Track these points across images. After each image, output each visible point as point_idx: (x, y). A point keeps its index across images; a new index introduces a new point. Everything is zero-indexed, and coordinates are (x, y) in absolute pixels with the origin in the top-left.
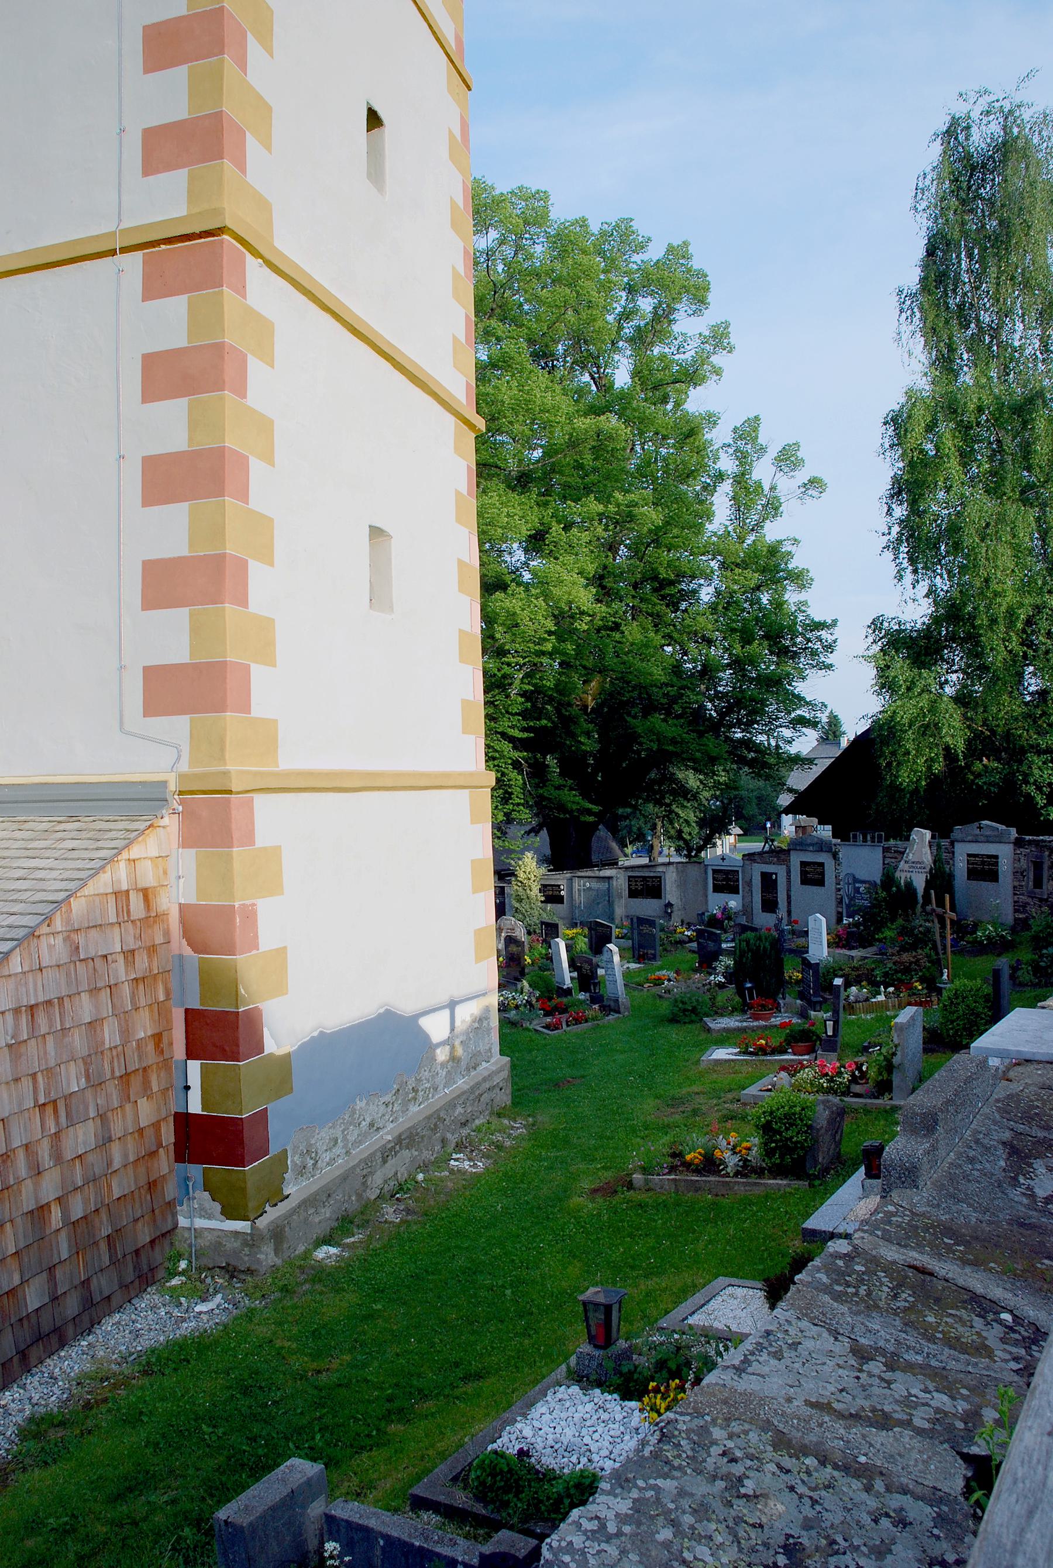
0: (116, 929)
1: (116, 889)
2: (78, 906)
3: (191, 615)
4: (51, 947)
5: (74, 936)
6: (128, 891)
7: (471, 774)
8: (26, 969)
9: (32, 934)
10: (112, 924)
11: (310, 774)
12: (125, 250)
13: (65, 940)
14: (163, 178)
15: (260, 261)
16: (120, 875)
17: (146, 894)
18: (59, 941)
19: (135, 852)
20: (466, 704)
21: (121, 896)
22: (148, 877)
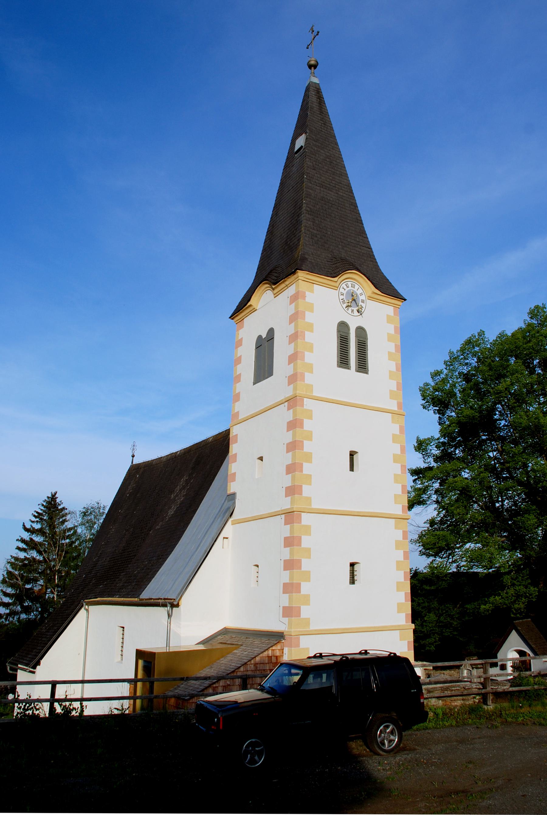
0: (268, 665)
1: (268, 655)
2: (258, 659)
3: (289, 596)
4: (250, 667)
5: (256, 665)
6: (271, 656)
7: (403, 625)
8: (244, 670)
9: (246, 663)
10: (267, 663)
11: (321, 630)
12: (281, 514)
13: (254, 666)
14: (287, 498)
15: (306, 513)
16: (270, 652)
17: (277, 657)
18: (252, 666)
19: (274, 648)
20: (400, 606)
21: (270, 658)
22: (278, 654)
